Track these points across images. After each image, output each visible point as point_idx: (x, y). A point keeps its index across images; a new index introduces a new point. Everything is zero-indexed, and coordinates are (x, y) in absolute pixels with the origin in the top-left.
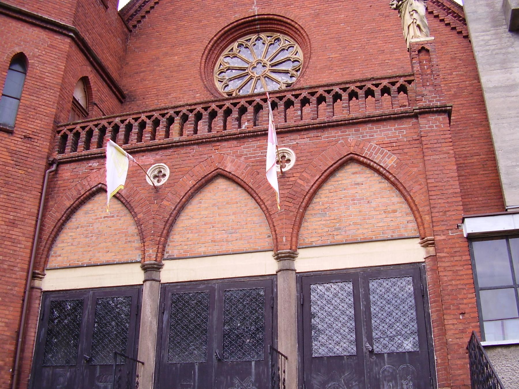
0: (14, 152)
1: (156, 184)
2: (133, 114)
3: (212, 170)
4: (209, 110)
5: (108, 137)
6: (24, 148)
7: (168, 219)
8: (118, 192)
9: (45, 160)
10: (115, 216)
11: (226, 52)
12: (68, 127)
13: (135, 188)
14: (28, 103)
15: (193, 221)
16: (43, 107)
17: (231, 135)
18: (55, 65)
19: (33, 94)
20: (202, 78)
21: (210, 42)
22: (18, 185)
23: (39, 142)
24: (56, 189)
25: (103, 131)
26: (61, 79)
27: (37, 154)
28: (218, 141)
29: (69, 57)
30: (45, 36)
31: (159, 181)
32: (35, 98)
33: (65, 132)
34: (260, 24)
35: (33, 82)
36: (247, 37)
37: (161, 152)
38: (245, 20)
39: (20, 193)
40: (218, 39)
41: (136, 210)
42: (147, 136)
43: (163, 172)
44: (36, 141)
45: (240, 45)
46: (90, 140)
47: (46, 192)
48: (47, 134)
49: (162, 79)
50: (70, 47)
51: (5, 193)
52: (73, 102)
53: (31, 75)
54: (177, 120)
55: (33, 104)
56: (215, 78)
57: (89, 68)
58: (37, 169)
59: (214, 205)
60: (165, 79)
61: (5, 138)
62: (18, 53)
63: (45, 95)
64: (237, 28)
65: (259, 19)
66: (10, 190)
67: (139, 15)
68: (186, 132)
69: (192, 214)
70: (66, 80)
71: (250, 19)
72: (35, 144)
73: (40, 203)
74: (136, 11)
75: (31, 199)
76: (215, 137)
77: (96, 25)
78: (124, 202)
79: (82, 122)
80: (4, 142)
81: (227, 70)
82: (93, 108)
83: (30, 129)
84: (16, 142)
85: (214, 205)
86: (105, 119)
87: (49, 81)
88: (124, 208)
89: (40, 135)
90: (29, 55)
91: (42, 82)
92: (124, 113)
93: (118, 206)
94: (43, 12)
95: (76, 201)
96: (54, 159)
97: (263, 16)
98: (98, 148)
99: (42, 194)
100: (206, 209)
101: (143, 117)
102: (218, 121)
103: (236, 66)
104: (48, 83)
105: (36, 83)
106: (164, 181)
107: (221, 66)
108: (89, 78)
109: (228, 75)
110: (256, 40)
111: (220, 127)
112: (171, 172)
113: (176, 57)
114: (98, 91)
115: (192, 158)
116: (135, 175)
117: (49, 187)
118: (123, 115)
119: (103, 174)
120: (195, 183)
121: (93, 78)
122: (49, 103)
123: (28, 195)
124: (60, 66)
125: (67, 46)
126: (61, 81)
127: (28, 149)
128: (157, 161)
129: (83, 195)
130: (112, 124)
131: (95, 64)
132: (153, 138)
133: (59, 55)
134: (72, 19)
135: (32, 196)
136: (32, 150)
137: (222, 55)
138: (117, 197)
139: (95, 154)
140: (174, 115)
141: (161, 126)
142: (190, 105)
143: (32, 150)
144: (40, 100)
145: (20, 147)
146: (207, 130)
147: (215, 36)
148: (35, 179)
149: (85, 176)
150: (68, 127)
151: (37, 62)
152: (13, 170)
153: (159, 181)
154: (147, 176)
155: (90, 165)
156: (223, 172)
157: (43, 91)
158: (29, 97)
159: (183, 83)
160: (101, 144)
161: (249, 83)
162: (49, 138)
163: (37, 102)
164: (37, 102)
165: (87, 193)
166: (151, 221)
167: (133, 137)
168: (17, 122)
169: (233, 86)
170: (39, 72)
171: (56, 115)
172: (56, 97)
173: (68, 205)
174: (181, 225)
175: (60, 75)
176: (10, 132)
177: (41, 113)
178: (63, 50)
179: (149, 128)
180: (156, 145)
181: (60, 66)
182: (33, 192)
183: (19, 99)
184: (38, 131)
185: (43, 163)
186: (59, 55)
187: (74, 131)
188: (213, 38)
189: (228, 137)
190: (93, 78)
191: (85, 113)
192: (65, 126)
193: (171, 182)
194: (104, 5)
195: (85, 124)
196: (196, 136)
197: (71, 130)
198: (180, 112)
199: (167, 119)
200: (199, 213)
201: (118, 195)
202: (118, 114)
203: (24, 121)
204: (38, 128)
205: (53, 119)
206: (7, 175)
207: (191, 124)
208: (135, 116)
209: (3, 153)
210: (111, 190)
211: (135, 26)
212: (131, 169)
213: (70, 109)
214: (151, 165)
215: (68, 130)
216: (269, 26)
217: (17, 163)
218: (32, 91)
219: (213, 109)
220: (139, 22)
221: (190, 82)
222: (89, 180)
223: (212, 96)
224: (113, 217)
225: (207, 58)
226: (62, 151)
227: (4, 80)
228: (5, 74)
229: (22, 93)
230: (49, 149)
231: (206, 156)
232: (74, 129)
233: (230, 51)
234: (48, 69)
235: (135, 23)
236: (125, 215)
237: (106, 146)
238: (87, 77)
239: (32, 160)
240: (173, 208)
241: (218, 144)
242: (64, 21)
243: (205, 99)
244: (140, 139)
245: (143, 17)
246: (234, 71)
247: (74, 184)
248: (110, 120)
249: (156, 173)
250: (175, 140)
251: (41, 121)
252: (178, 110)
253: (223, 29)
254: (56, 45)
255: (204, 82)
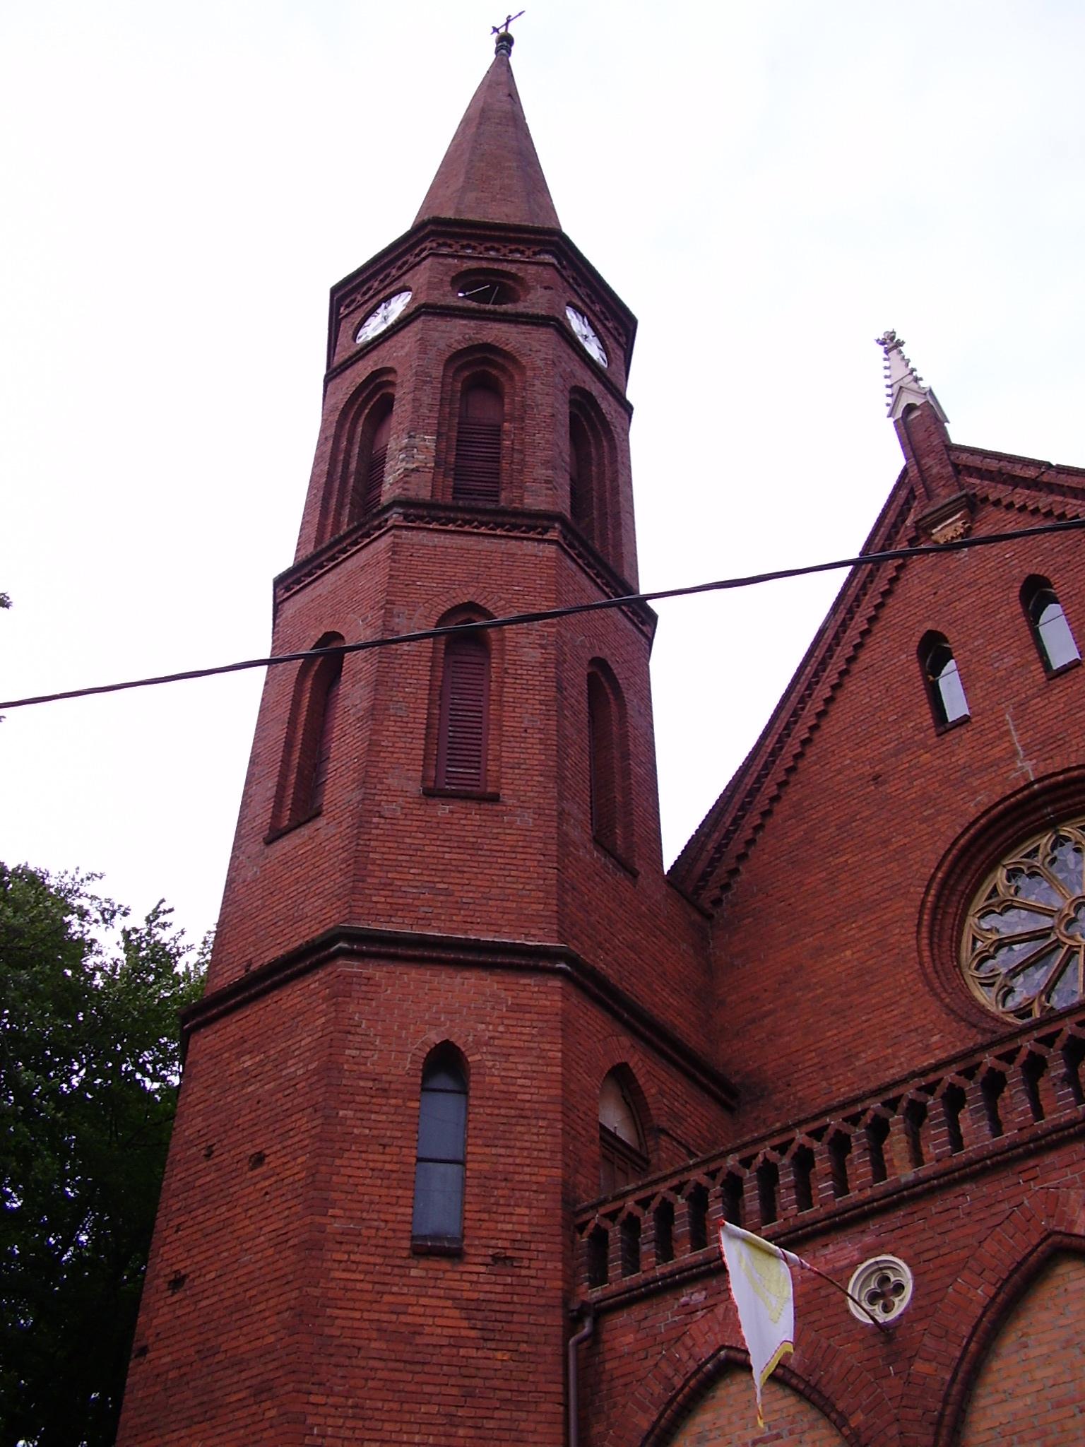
0: (473, 1305)
1: (882, 1318)
2: (771, 1135)
3: (1035, 1242)
4: (980, 1074)
5: (716, 1212)
6: (499, 1289)
7: (942, 1415)
8: (780, 1365)
9: (559, 1312)
10: (785, 1433)
11: (980, 902)
12: (603, 1210)
13: (824, 1344)
14: (485, 1166)
15: (1018, 1405)
16: (527, 1170)
17: (1062, 1129)
18: (534, 1053)
19: (496, 1142)
20: (932, 989)
21: (928, 887)
22: (500, 1394)
23: (534, 1264)
24: (604, 1387)
25: (699, 1199)
26: (559, 1085)
27: (534, 1300)
28: (1030, 1154)
29: (567, 1026)
30: (496, 986)
31: (887, 1309)
32: (502, 1151)
33: (597, 1226)
34: (1051, 802)
35: (488, 1110)
36: (1028, 847)
37: (873, 1225)
38: (1007, 803)
39: (507, 1415)
40: (948, 875)
41: (840, 1406)
42: (823, 1187)
43: (893, 1279)
44: (526, 1263)
45: (1013, 874)
46: (670, 1231)
47: (578, 1395)
48: (551, 1239)
49: (826, 1021)
50: (565, 998)
51: (470, 1423)
52: (602, 1138)
53: (479, 1094)
54: (897, 1122)
55: (501, 1168)
56: (969, 981)
57: (625, 1041)
58: (543, 1339)
59: (1068, 1344)
60: (833, 1018)
61: (445, 1271)
62: (437, 1046)
63: (526, 1137)
64: (992, 831)
65: (1044, 791)
66: (480, 1413)
67: (721, 870)
68: (930, 1150)
69: (1007, 1385)
70: (572, 1086)
71: (1019, 796)
72: (524, 1272)
73: (566, 1434)
74: (712, 862)
75: (539, 1428)
76: (1018, 1146)
77: (619, 926)
78: (802, 1387)
79: (639, 1189)
80: (444, 1284)
81: (997, 950)
82: (657, 1143)
83: (504, 1235)
84: (474, 1278)
85: (1068, 1344)
86: (696, 1166)
87: (527, 1097)
88: (805, 1406)
89: (533, 1246)
90: (465, 1043)
91: (512, 1104)
92: (747, 1138)
93: (787, 1403)
94: (478, 927)
95: (665, 1410)
96: (584, 1303)
97: (1053, 780)
98: (694, 1249)
99: (567, 1406)
100: (1047, 1360)
101: (800, 1136)
102: (1015, 1100)
103: (1019, 930)
104: (527, 1105)
105: (496, 1111)
106: (901, 1304)
107: (979, 944)
108: (631, 1065)
109: (1003, 962)
110: (1053, 848)
111: (1023, 1113)
112: (916, 1275)
113: (848, 953)
114: (662, 1093)
115: (966, 1220)
116: (816, 1302)
117: (582, 1384)
118: (745, 1145)
119: (724, 1319)
120: (993, 1290)
121: (640, 1063)
122: (542, 1155)
123: (532, 1417)
124: (550, 1054)
125: (556, 998)
126: (559, 1092)
127: (508, 1289)
128: (868, 1252)
129: (682, 1388)
130: (721, 1176)
131: (637, 1025)
132: (842, 1187)
133: (540, 1025)
134: (555, 927)
135: (542, 1418)
136: (518, 1290)
137: (971, 912)
138: (781, 1377)
139: (691, 1268)
140: (884, 1113)
141: (855, 1152)
142: (923, 1073)
143: (518, 1290)
144: (516, 1152)
145: (487, 1288)
146: (987, 1131)
147: (938, 869)
148: (541, 1368)
149: (674, 1334)
150: (603, 1210)
151: (489, 1057)
152: (480, 1354)
153: (887, 1309)
154: (850, 1301)
155: (683, 1300)
156: (1067, 1240)
157: (519, 1128)
158: (487, 1150)
159: (885, 1016)
160: (702, 1236)
161: (1069, 970)
162: (559, 1248)
163: (510, 1160)
164: (510, 1160)
165: (692, 1383)
166: (893, 1430)
167: (787, 1198)
168: (468, 1223)
169: (1024, 990)
170: (498, 1080)
171: (565, 1184)
172: (553, 1136)
173: (646, 1426)
174: (983, 1425)
175: (553, 1077)
176: (455, 1254)
177: (524, 1186)
178: (549, 1010)
179: (822, 1164)
180: (854, 1208)
181: (550, 1054)
182: (544, 1407)
183: (462, 1163)
184: (528, 1237)
185: (556, 1320)
186: (540, 1025)
187: (623, 1216)
188: (934, 876)
189: (1054, 1137)
190: (640, 1064)
191: (640, 1162)
192: (594, 1207)
193: (921, 1303)
194: (626, 869)
195: (648, 1192)
196: (961, 1156)
197: (612, 1216)
198: (898, 1099)
199: (868, 1127)
200: (1028, 1376)
201: (780, 1371)
202: (729, 1146)
203: (485, 1216)
204: (526, 1228)
205: (560, 1197)
206: (464, 1371)
207: (938, 1125)
208: (777, 1141)
209: (446, 1312)
210: (762, 1360)
211: (717, 902)
212: (804, 1295)
213: (598, 1159)
214: (853, 1266)
215: (605, 1216)
216: (1077, 799)
217: (487, 1335)
218: (490, 1134)
219: (991, 1070)
220: (726, 887)
221: (903, 1009)
222: (689, 1343)
223: (975, 1031)
224: (778, 1436)
225: (931, 932)
226: (599, 1277)
227: (416, 1120)
228: (417, 1104)
229: (466, 1144)
230: (564, 1281)
231: (1005, 1206)
232: (621, 1209)
233: (989, 898)
234: (521, 1067)
235: (717, 892)
236: (812, 1427)
237: (718, 1240)
238: (626, 1064)
239: (525, 1318)
240: (948, 1377)
241: (1031, 1163)
242: (534, 936)
243: (960, 1048)
244: (805, 1200)
245: (734, 872)
246: (1016, 947)
247: (650, 1362)
248: (713, 1166)
249: (873, 1285)
250: (903, 1180)
251: (530, 1207)
252: (891, 1095)
253: (953, 844)
254: (525, 1002)
255: (942, 1000)
